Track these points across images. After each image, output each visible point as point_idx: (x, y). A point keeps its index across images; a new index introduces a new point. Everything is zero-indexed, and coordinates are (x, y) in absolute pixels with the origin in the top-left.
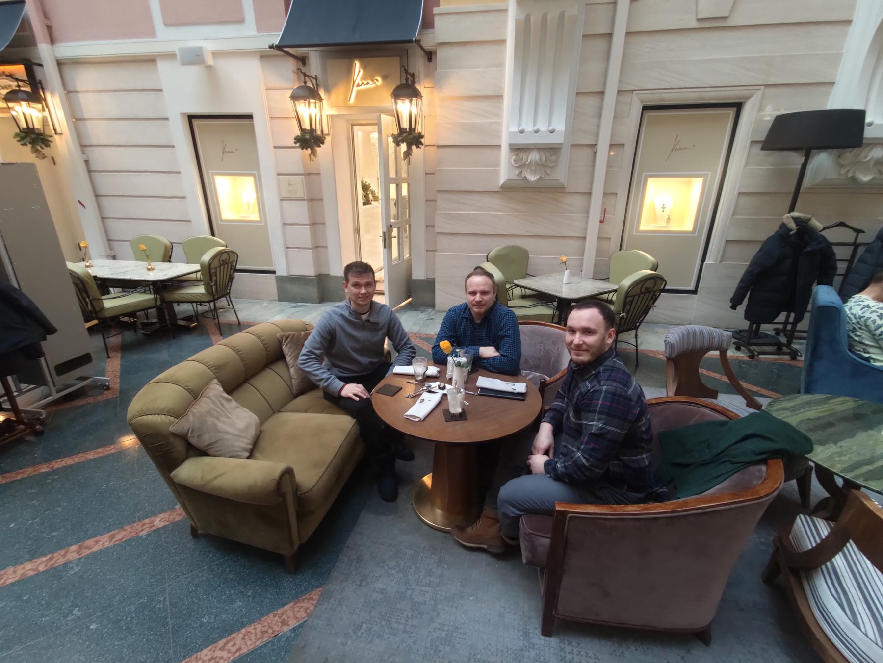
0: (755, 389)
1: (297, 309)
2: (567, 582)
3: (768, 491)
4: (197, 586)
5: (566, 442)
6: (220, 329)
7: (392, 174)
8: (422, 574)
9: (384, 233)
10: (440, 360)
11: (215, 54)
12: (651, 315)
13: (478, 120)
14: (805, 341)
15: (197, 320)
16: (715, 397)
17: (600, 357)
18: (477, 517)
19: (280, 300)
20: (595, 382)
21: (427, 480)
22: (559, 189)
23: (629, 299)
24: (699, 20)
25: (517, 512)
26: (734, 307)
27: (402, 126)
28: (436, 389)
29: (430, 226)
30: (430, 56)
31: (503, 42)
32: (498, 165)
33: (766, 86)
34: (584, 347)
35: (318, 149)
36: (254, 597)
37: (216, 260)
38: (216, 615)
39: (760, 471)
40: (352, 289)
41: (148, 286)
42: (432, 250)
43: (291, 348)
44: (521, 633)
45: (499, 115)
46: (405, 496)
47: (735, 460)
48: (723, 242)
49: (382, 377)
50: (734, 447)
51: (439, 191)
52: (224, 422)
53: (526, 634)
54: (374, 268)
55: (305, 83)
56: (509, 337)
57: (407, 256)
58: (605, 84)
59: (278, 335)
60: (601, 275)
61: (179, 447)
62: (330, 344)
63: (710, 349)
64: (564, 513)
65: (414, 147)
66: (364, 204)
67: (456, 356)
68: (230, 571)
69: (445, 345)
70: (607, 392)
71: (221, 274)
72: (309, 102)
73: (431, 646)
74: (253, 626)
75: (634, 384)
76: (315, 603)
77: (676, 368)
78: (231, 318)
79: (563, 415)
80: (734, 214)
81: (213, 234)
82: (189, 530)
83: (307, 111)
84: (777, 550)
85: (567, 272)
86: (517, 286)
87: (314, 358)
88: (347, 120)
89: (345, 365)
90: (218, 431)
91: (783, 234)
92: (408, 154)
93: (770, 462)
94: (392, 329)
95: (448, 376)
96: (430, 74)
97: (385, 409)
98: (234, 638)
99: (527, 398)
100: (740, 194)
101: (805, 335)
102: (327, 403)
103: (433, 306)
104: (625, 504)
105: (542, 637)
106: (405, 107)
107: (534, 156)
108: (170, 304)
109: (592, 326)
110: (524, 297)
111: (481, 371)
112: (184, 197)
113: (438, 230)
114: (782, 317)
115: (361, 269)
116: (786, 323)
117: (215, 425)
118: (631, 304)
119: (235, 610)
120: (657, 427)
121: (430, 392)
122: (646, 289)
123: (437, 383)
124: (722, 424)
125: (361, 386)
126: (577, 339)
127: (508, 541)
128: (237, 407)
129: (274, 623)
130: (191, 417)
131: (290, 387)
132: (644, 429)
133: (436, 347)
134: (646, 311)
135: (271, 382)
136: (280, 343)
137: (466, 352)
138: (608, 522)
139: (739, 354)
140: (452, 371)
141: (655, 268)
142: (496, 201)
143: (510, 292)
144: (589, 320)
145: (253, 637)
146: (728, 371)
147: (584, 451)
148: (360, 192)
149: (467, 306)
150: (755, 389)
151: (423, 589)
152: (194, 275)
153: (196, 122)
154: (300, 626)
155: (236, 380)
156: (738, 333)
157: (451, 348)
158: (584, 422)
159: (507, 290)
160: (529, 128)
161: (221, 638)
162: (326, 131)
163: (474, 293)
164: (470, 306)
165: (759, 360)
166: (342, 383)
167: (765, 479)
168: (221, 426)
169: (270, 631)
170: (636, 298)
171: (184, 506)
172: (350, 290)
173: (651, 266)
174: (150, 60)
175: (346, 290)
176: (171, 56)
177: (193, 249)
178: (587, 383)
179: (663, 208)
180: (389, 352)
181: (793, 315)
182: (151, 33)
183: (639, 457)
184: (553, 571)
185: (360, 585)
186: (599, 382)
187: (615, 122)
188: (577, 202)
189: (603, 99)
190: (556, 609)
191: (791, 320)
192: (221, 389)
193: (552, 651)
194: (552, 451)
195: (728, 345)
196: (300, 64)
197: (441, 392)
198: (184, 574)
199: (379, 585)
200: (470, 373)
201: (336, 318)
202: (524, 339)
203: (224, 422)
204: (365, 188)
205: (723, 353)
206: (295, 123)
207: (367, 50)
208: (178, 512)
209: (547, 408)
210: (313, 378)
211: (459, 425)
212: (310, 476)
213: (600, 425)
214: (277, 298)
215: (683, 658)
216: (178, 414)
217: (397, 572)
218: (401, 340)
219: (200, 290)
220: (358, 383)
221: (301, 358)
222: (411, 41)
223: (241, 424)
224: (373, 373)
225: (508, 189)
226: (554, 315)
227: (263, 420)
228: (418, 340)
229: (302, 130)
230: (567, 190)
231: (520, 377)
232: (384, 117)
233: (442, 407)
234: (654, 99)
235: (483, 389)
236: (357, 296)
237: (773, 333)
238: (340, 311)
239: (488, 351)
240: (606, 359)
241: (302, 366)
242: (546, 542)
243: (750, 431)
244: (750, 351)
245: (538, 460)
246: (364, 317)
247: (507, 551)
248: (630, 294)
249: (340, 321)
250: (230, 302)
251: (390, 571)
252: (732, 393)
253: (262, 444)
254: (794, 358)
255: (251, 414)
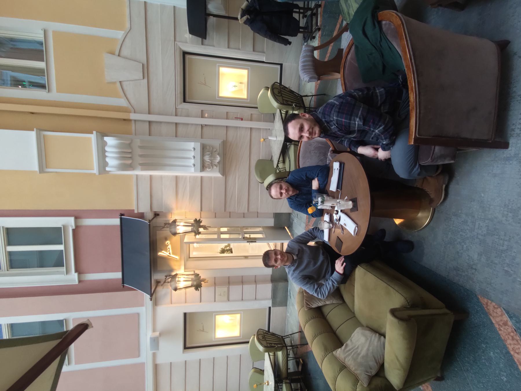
1: (292, 295)
2: (466, 135)
3: (398, 19)
5: (369, 138)
6: (304, 345)
7: (215, 236)
9: (248, 242)
10: (320, 213)
11: (154, 330)
12: (294, 89)
13: (188, 189)
14: (310, 2)
15: (299, 358)
16: (343, 49)
17: (317, 121)
18: (422, 190)
20: (332, 123)
21: (398, 221)
22: (225, 144)
23: (285, 103)
24: (143, 78)
25: (417, 166)
26: (290, 43)
28: (338, 216)
29: (244, 216)
30: (156, 215)
34: (311, 130)
35: (202, 278)
36: (487, 343)
37: (262, 342)
38: (501, 370)
39: (385, 24)
41: (278, 386)
42: (258, 215)
43: (314, 303)
44: (507, 162)
45: (185, 178)
46: (409, 236)
47: (379, 39)
50: (370, 40)
51: (225, 210)
52: (361, 351)
53: (508, 159)
54: (268, 249)
55: (168, 282)
56: (306, 174)
57: (260, 229)
59: (306, 310)
60: (271, 118)
61: (378, 382)
62: (311, 279)
63: (313, 56)
64: (416, 139)
65: (201, 224)
66: (232, 252)
67: (318, 203)
69: (310, 210)
70: (337, 116)
71: (271, 340)
72: (178, 281)
74: (509, 346)
75: (332, 101)
76: (490, 301)
77: (324, 74)
78: (297, 336)
79: (352, 140)
80: (239, 49)
81: (248, 342)
82: (438, 382)
83: (182, 282)
84: (441, 5)
86: (277, 166)
87: (320, 289)
88: (187, 260)
89: (324, 271)
90: (367, 354)
91: (250, 22)
92: (205, 227)
93: (380, 19)
94: (302, 241)
95: (330, 208)
96: (165, 215)
97: (350, 247)
99: (343, 161)
101: (306, 2)
102: (348, 283)
103: (290, 214)
104: (409, 102)
105: (510, 148)
106: (181, 229)
107: (207, 158)
109: (298, 126)
110: (284, 162)
111: (326, 188)
112: (227, 357)
113: (246, 211)
114: (296, 16)
115: (267, 257)
116: (299, 13)
117: (363, 357)
118: (288, 101)
121: (339, 219)
123: (334, 215)
124: (356, 47)
125: (337, 261)
126: (306, 134)
127: (439, 171)
128: (351, 340)
130: (358, 372)
131: (339, 304)
132: (360, 93)
133: (313, 215)
135: (335, 316)
136: (311, 309)
137: (315, 197)
138: (422, 112)
140: (327, 206)
141: (267, 88)
142: (230, 179)
143: (281, 170)
144: (295, 128)
145: (517, 347)
146: (327, 44)
147: (375, 128)
148: (225, 255)
149: (289, 198)
151: (477, 226)
152: (271, 357)
154: (508, 313)
155: (335, 340)
156: (306, 39)
157: (313, 207)
158: (356, 129)
159: (280, 171)
160: (192, 161)
162: (192, 273)
163: (281, 194)
164: (289, 196)
165: (321, 25)
166: (335, 272)
168: (363, 352)
169: (512, 334)
170: (284, 98)
171: (420, 384)
172: (279, 264)
174: (156, 367)
175: (279, 267)
176: (154, 355)
177: (257, 356)
178: (332, 128)
179: (235, 86)
180: (316, 243)
181: (295, 10)
183: (379, 94)
184: (449, 151)
185: (476, 270)
186: (331, 121)
187: (191, 116)
188: (231, 133)
190: (488, 140)
191: (298, 10)
192: (340, 349)
194: (376, 146)
195: (310, 46)
197: (340, 213)
199: (476, 257)
201: (295, 275)
202: (308, 164)
203: (361, 351)
204: (223, 251)
205: (315, 48)
207: (154, 246)
209: (349, 150)
212: (396, 299)
213: (358, 119)
214: (285, 307)
216: (356, 380)
217: (465, 244)
218: (309, 236)
219: (280, 354)
220: (335, 263)
221: (320, 297)
222: (150, 225)
223: (362, 340)
224: (329, 253)
225: (224, 172)
226: (294, 145)
227: (359, 324)
229: (192, 286)
230: (225, 139)
231: (330, 165)
233: (349, 213)
235: (338, 187)
236: (282, 260)
237: (305, 19)
238: (291, 272)
240: (318, 117)
241: (325, 297)
242: (437, 148)
243: (361, 32)
244: (315, 31)
245: (382, 154)
246: (295, 258)
247: (448, 172)
249: (297, 272)
251: (465, 249)
252: (340, 41)
254: (320, 6)
255: (355, 332)
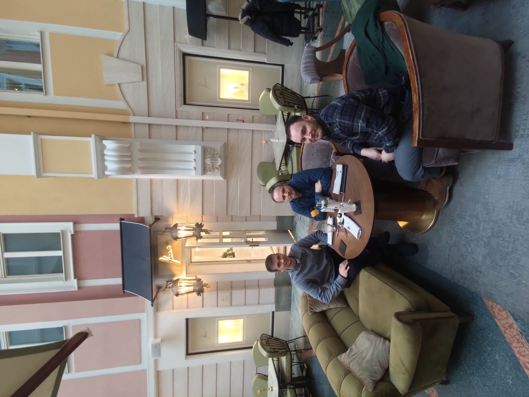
0: (340, 26)
1: (295, 299)
4: (485, 385)
5: (373, 140)
6: (308, 349)
7: (217, 241)
8: (470, 229)
9: (250, 246)
10: (324, 216)
11: (156, 337)
12: (296, 90)
14: (312, 2)
16: (345, 50)
17: (319, 123)
18: (426, 192)
19: (290, 310)
20: (334, 125)
21: (402, 224)
22: (226, 146)
23: (287, 104)
24: (143, 80)
26: (291, 44)
27: (192, 235)
28: (342, 219)
29: (246, 219)
30: (157, 219)
31: (151, 180)
32: (213, 180)
33: (174, 42)
34: (313, 132)
35: (204, 283)
36: (493, 346)
38: (507, 374)
39: (388, 25)
40: (281, 267)
41: (282, 392)
44: (511, 164)
45: (187, 181)
46: (414, 238)
47: (382, 40)
48: (255, 54)
49: (334, 251)
52: (366, 355)
53: (512, 160)
55: (170, 288)
56: (309, 176)
58: (172, 126)
59: (310, 314)
60: (273, 120)
61: (383, 386)
62: (315, 283)
63: (315, 57)
64: (419, 141)
65: (203, 228)
66: (234, 256)
67: (321, 206)
68: (473, 361)
69: (313, 214)
70: (340, 118)
71: (275, 345)
72: (180, 286)
73: (524, 225)
74: (515, 349)
76: (495, 304)
78: (301, 341)
79: (355, 143)
80: (240, 50)
81: (251, 348)
82: (444, 386)
83: (184, 288)
84: (443, 5)
85: (272, 140)
86: (280, 168)
87: (324, 293)
88: (189, 265)
89: (328, 273)
92: (206, 232)
94: (306, 244)
95: (333, 211)
96: (166, 219)
97: (354, 251)
98: (523, 363)
99: (346, 164)
100: (229, 48)
101: (307, 3)
104: (412, 103)
105: (514, 150)
106: (182, 233)
107: (208, 161)
108: (293, 380)
109: (301, 128)
110: (286, 164)
111: (330, 191)
113: (248, 215)
114: (297, 16)
116: (301, 13)
117: (368, 361)
118: (290, 103)
119: (502, 360)
120: (361, 86)
122: (281, 95)
123: (338, 218)
124: (359, 48)
125: (340, 265)
126: (308, 137)
127: (443, 173)
128: (356, 345)
129: (511, 333)
130: (363, 377)
131: (343, 309)
132: (363, 95)
133: (316, 218)
134: (294, 93)
135: (340, 320)
136: (315, 313)
138: (425, 113)
139: (319, 37)
140: (330, 209)
141: (269, 90)
142: (232, 182)
143: (284, 172)
144: (297, 131)
145: (522, 349)
147: (378, 130)
150: (340, 26)
151: (481, 229)
152: (275, 362)
153: (190, 351)
154: (513, 315)
155: (339, 345)
156: (307, 40)
157: (316, 210)
158: (359, 131)
159: (282, 174)
160: (193, 164)
161: (523, 372)
162: (194, 278)
163: (284, 197)
164: (292, 199)
165: (323, 25)
166: (339, 276)
167: (393, 22)
168: (368, 357)
169: (517, 337)
171: (426, 387)
172: (282, 268)
173: (268, 92)
174: (158, 374)
175: (282, 271)
177: (260, 362)
178: (335, 130)
179: (236, 88)
181: (296, 10)
182: (144, 372)
183: (381, 96)
184: (461, 147)
185: (480, 272)
186: (334, 123)
187: (192, 119)
188: (233, 136)
189: (180, 126)
191: (299, 10)
193: (524, 143)
194: (379, 149)
195: (312, 47)
196: (161, 290)
197: (343, 216)
198: (476, 393)
200: (331, 198)
201: (299, 279)
203: (366, 355)
204: (225, 255)
205: (317, 49)
206: (190, 295)
207: (155, 251)
208: (431, 392)
209: (352, 152)
210: (336, 294)
211: (364, 205)
212: (401, 302)
213: (361, 121)
215: (524, 57)
216: (361, 385)
217: (470, 246)
219: (284, 359)
221: (324, 301)
222: (150, 229)
223: (367, 344)
224: (333, 257)
225: (226, 175)
227: (363, 328)
228: (313, 227)
230: (226, 142)
231: (333, 167)
232: (187, 245)
233: (353, 216)
234: (180, 99)
235: (341, 190)
236: (285, 265)
237: (307, 19)
239: (318, 187)
240: (320, 119)
242: (441, 150)
243: (363, 34)
244: (317, 31)
245: (385, 156)
246: (298, 262)
247: (452, 174)
248: (284, 104)
249: (301, 276)
250: (291, 341)
251: (469, 251)
253: (380, 330)
254: (321, 6)
